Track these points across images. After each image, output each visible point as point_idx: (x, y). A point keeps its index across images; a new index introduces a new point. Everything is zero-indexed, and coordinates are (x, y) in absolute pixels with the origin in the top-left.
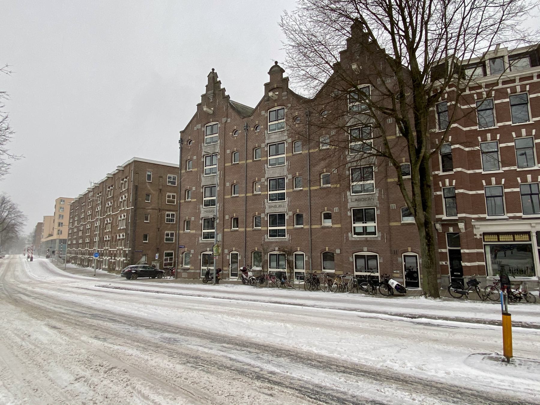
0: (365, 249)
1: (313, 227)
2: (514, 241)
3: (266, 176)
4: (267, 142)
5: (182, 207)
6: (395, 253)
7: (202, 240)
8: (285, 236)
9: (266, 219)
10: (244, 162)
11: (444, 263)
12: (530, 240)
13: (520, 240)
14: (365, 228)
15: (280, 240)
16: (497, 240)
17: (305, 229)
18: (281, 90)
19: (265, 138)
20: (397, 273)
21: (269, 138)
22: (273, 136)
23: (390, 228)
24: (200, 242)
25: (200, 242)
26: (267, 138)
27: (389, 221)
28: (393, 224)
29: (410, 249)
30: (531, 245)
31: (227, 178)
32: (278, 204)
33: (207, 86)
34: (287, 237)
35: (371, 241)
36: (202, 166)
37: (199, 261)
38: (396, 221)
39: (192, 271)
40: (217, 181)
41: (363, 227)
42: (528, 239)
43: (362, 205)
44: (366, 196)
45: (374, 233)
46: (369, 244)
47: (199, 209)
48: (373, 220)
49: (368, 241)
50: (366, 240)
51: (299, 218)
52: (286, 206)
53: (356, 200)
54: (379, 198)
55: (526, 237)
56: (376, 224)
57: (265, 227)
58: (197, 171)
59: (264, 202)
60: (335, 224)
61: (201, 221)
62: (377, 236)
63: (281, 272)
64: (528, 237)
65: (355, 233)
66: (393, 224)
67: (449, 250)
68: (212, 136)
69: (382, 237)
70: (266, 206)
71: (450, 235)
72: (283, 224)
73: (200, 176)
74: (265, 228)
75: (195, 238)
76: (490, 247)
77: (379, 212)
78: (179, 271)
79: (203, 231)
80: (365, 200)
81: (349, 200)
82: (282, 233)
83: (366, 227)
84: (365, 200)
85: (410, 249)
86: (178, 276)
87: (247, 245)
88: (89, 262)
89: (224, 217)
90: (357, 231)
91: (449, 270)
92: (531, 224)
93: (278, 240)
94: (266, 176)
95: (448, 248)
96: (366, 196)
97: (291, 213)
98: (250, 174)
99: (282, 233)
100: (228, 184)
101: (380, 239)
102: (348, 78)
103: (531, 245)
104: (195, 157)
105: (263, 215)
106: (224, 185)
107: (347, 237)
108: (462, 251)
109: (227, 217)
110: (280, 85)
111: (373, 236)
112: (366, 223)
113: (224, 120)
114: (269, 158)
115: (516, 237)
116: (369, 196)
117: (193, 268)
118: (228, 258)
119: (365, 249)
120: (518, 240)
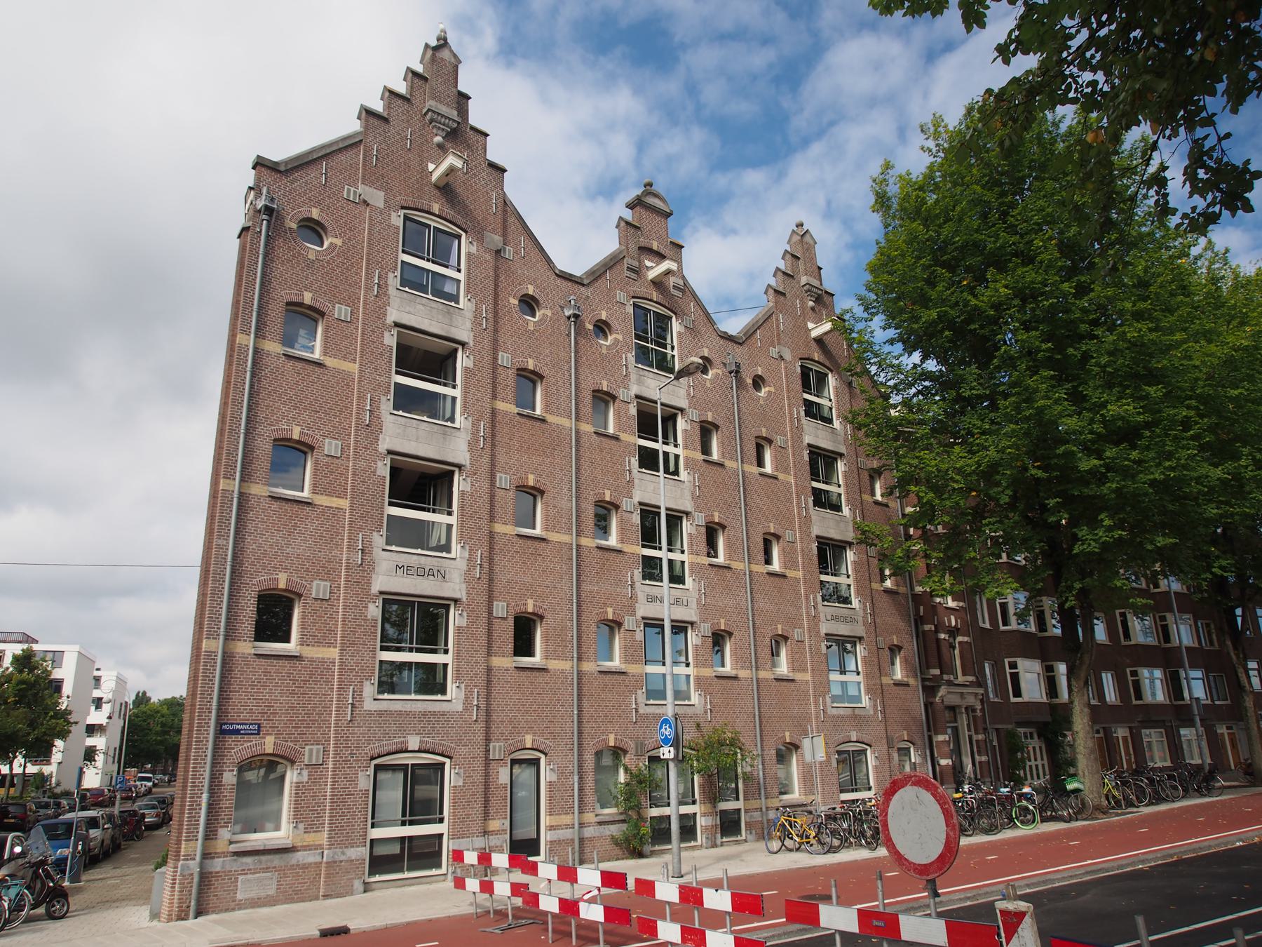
12: (956, 721)
25: (369, 705)
49: (855, 716)
109: (500, 609)
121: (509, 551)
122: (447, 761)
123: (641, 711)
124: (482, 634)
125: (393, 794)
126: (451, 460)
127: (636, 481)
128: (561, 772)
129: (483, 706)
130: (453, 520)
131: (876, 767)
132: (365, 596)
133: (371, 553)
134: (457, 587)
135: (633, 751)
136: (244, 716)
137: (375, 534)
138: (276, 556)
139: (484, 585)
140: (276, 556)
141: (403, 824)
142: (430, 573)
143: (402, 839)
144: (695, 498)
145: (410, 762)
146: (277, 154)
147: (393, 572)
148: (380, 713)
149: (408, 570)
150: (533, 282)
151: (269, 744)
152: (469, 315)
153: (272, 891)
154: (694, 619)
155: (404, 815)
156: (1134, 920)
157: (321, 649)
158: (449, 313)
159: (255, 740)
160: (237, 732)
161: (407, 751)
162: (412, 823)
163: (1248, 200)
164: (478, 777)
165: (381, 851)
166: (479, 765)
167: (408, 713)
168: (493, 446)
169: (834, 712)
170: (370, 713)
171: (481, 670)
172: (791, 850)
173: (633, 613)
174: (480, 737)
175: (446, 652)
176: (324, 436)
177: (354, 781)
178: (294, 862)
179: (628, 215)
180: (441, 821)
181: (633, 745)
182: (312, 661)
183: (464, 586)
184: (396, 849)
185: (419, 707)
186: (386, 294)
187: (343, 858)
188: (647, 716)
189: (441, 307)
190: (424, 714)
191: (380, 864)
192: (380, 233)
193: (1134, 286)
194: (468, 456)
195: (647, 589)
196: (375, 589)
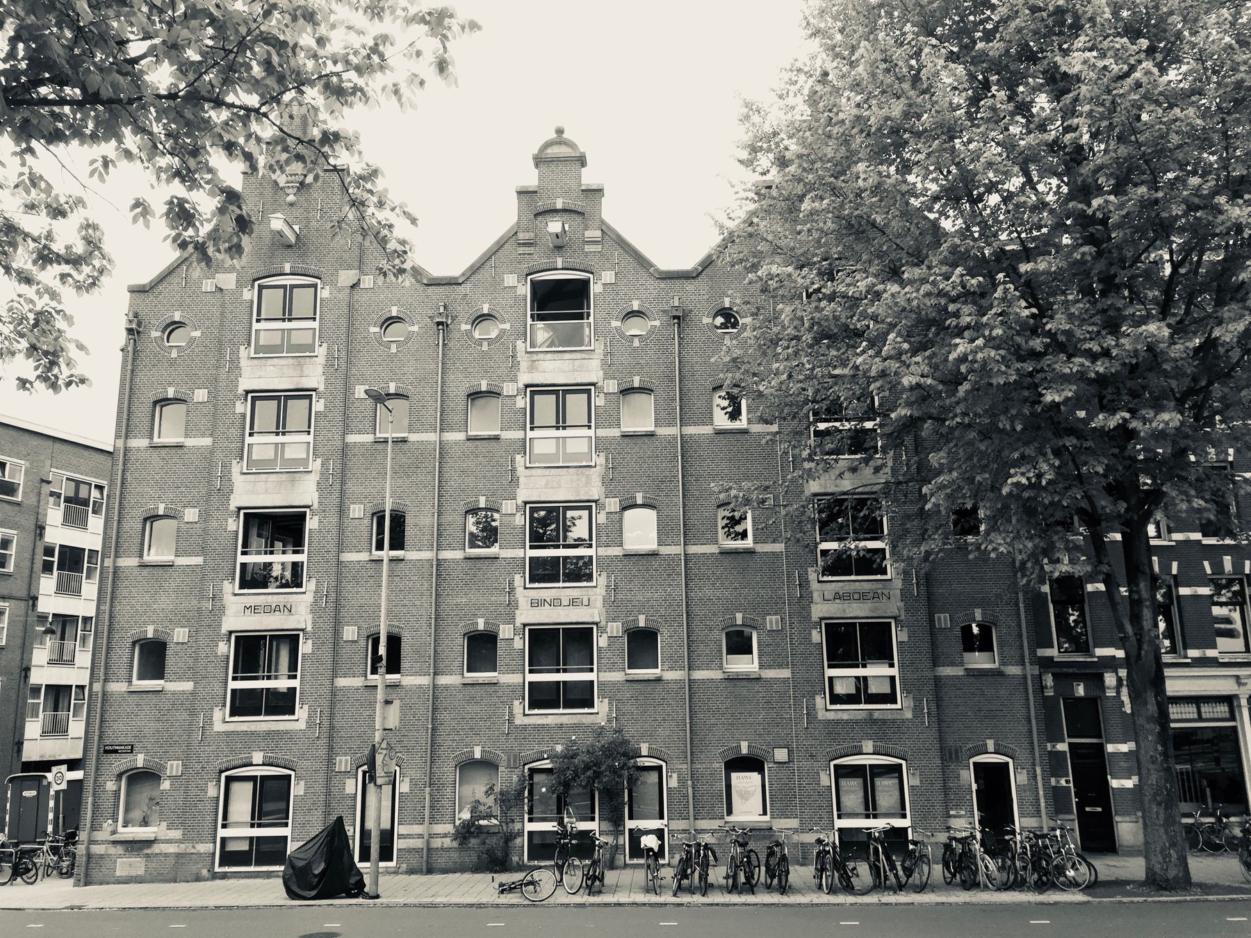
0: (868, 746)
1: (699, 675)
2: (1200, 719)
3: (523, 494)
4: (525, 378)
5: (122, 584)
10: (432, 437)
11: (1063, 782)
12: (1233, 718)
13: (1212, 716)
14: (862, 682)
16: (1196, 716)
17: (668, 682)
20: (960, 816)
23: (937, 680)
24: (218, 727)
25: (218, 727)
26: (524, 365)
28: (947, 671)
29: (991, 744)
30: (1235, 728)
31: (351, 487)
35: (884, 721)
36: (234, 432)
37: (209, 807)
38: (952, 664)
39: (172, 849)
41: (857, 678)
42: (1227, 715)
43: (857, 611)
44: (867, 586)
45: (890, 698)
46: (876, 727)
48: (884, 655)
49: (875, 721)
50: (871, 721)
51: (641, 644)
53: (837, 596)
54: (905, 594)
55: (1223, 709)
56: (894, 671)
58: (211, 451)
60: (770, 667)
62: (899, 706)
63: (894, 830)
64: (1227, 709)
65: (836, 699)
66: (947, 671)
68: (287, 325)
69: (917, 709)
70: (521, 600)
71: (1074, 704)
72: (587, 663)
73: (226, 467)
75: (193, 713)
77: (904, 637)
78: (97, 849)
81: (816, 596)
83: (865, 678)
85: (991, 744)
86: (95, 873)
87: (439, 740)
88: (751, 830)
89: (337, 633)
90: (840, 689)
91: (1074, 800)
92: (1237, 677)
95: (1067, 740)
96: (867, 586)
97: (615, 628)
98: (454, 481)
101: (909, 715)
102: (770, 238)
103: (1235, 728)
105: (505, 632)
106: (342, 511)
107: (811, 710)
108: (1110, 748)
110: (579, 205)
111: (889, 706)
112: (864, 666)
113: (346, 277)
114: (530, 434)
115: (1203, 710)
117: (176, 834)
119: (868, 746)
120: (1208, 716)
121: (362, 577)
122: (292, 773)
124: (926, 647)
125: (243, 798)
127: (522, 480)
130: (241, 559)
134: (302, 619)
135: (505, 764)
136: (122, 740)
138: (145, 613)
139: (330, 611)
140: (145, 613)
141: (252, 826)
142: (277, 609)
143: (251, 839)
145: (259, 774)
146: (145, 279)
147: (241, 613)
149: (254, 609)
151: (140, 760)
153: (141, 871)
154: (597, 619)
155: (253, 818)
158: (300, 365)
159: (130, 757)
160: (116, 751)
161: (251, 765)
162: (260, 826)
164: (319, 787)
165: (232, 847)
166: (321, 776)
167: (253, 733)
169: (831, 716)
171: (325, 691)
172: (73, 865)
173: (512, 620)
174: (322, 752)
177: (205, 791)
178: (157, 851)
179: (589, 177)
180: (286, 825)
181: (504, 757)
182: (174, 693)
184: (244, 847)
185: (264, 727)
186: (238, 367)
187: (193, 851)
188: (524, 727)
189: (291, 361)
190: (269, 733)
191: (229, 858)
192: (232, 312)
193: (301, 82)
196: (224, 630)
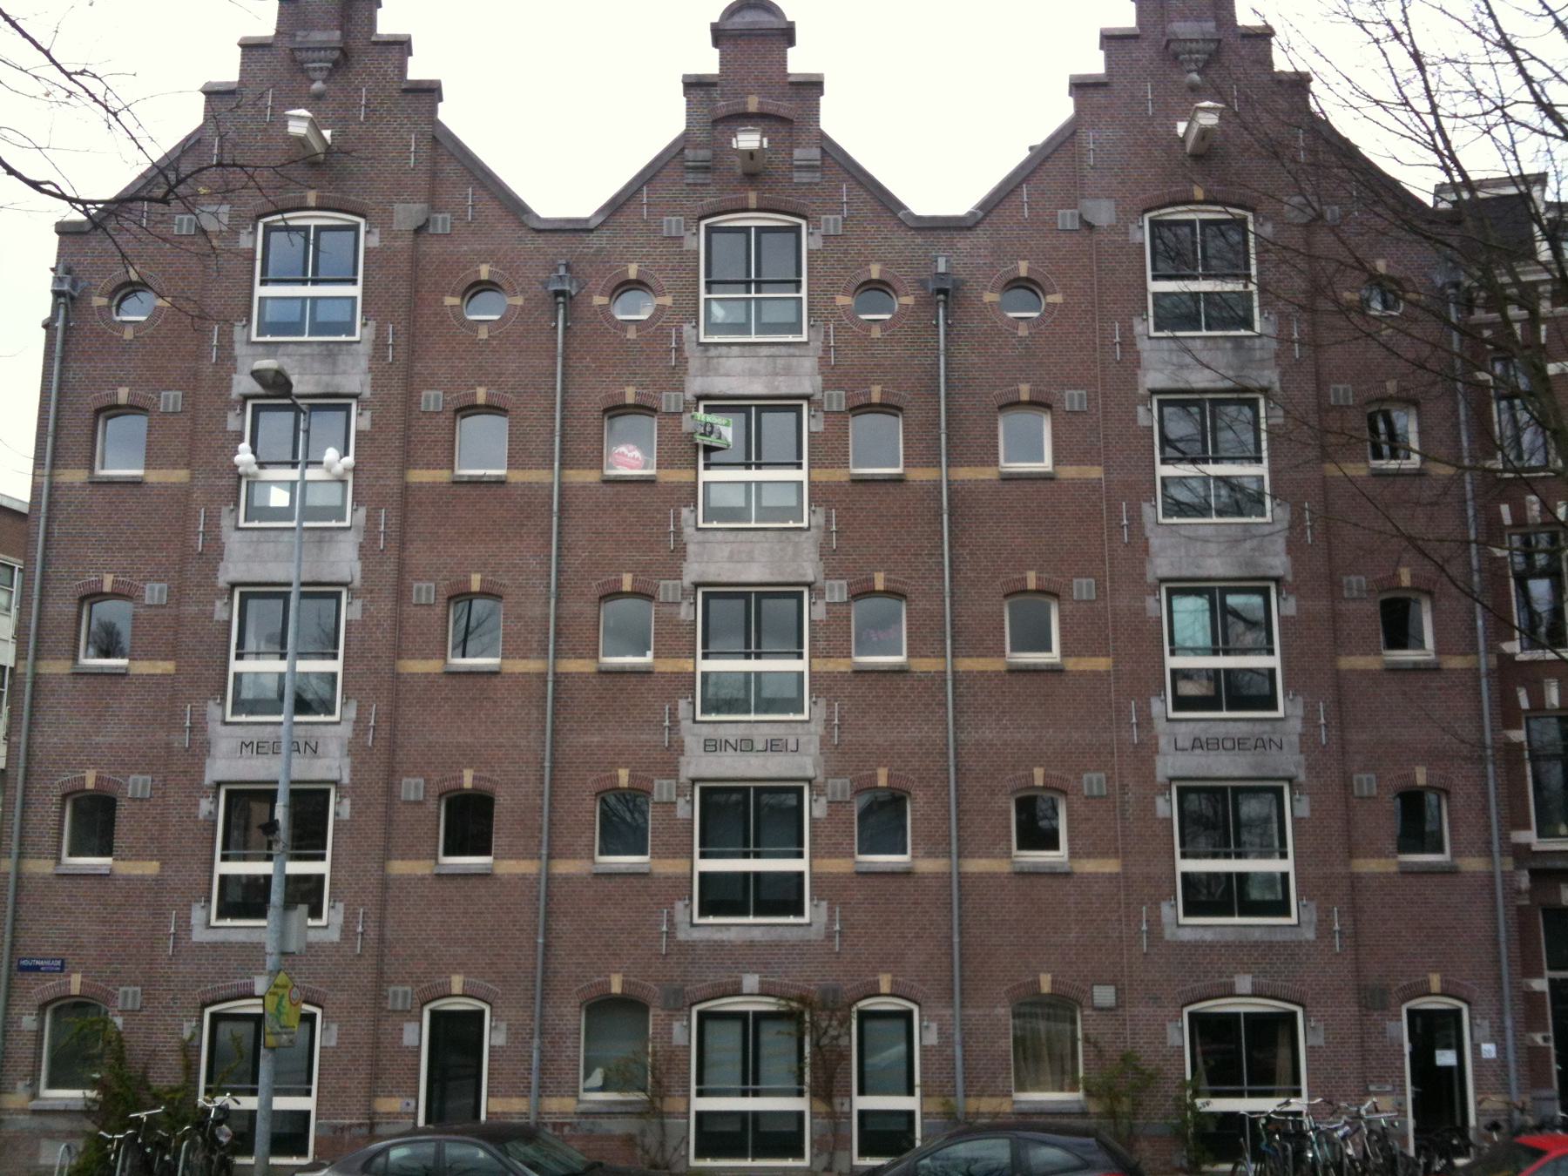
3: (692, 571)
6: (1373, 1000)
7: (209, 926)
8: (799, 912)
9: (682, 811)
15: (774, 935)
17: (924, 876)
18: (783, 131)
19: (682, 361)
21: (706, 370)
22: (735, 363)
24: (199, 935)
25: (199, 935)
26: (694, 364)
27: (1351, 854)
28: (418, 476)
32: (761, 735)
33: (441, 100)
34: (813, 913)
40: (344, 561)
47: (198, 727)
51: (882, 818)
52: (814, 748)
54: (1307, 742)
57: (675, 855)
59: (673, 713)
60: (1089, 855)
61: (205, 806)
62: (1293, 920)
66: (418, 476)
67: (1552, 982)
69: (1323, 928)
74: (670, 867)
76: (792, 1133)
79: (223, 868)
80: (1239, 744)
81: (1163, 742)
82: (780, 896)
84: (1239, 744)
85: (1435, 982)
93: (757, 934)
94: (692, 571)
95: (1548, 973)
96: (1244, 729)
99: (780, 896)
100: (424, 591)
101: (1309, 934)
104: (171, 399)
105: (662, 789)
109: (411, 787)
113: (407, 214)
116: (1258, 728)
118: (409, 1038)
123: (681, 936)
126: (334, 579)
127: (691, 548)
128: (513, 1033)
129: (372, 934)
131: (1559, 1072)
132: (195, 787)
133: (204, 730)
137: (211, 703)
144: (825, 553)
148: (215, 946)
150: (487, 257)
152: (365, 349)
156: (152, 858)
157: (140, 864)
163: (249, 810)
168: (402, 545)
170: (201, 945)
173: (674, 773)
175: (1284, 855)
176: (145, 580)
183: (347, 761)
188: (691, 946)
194: (358, 566)
195: (706, 731)
